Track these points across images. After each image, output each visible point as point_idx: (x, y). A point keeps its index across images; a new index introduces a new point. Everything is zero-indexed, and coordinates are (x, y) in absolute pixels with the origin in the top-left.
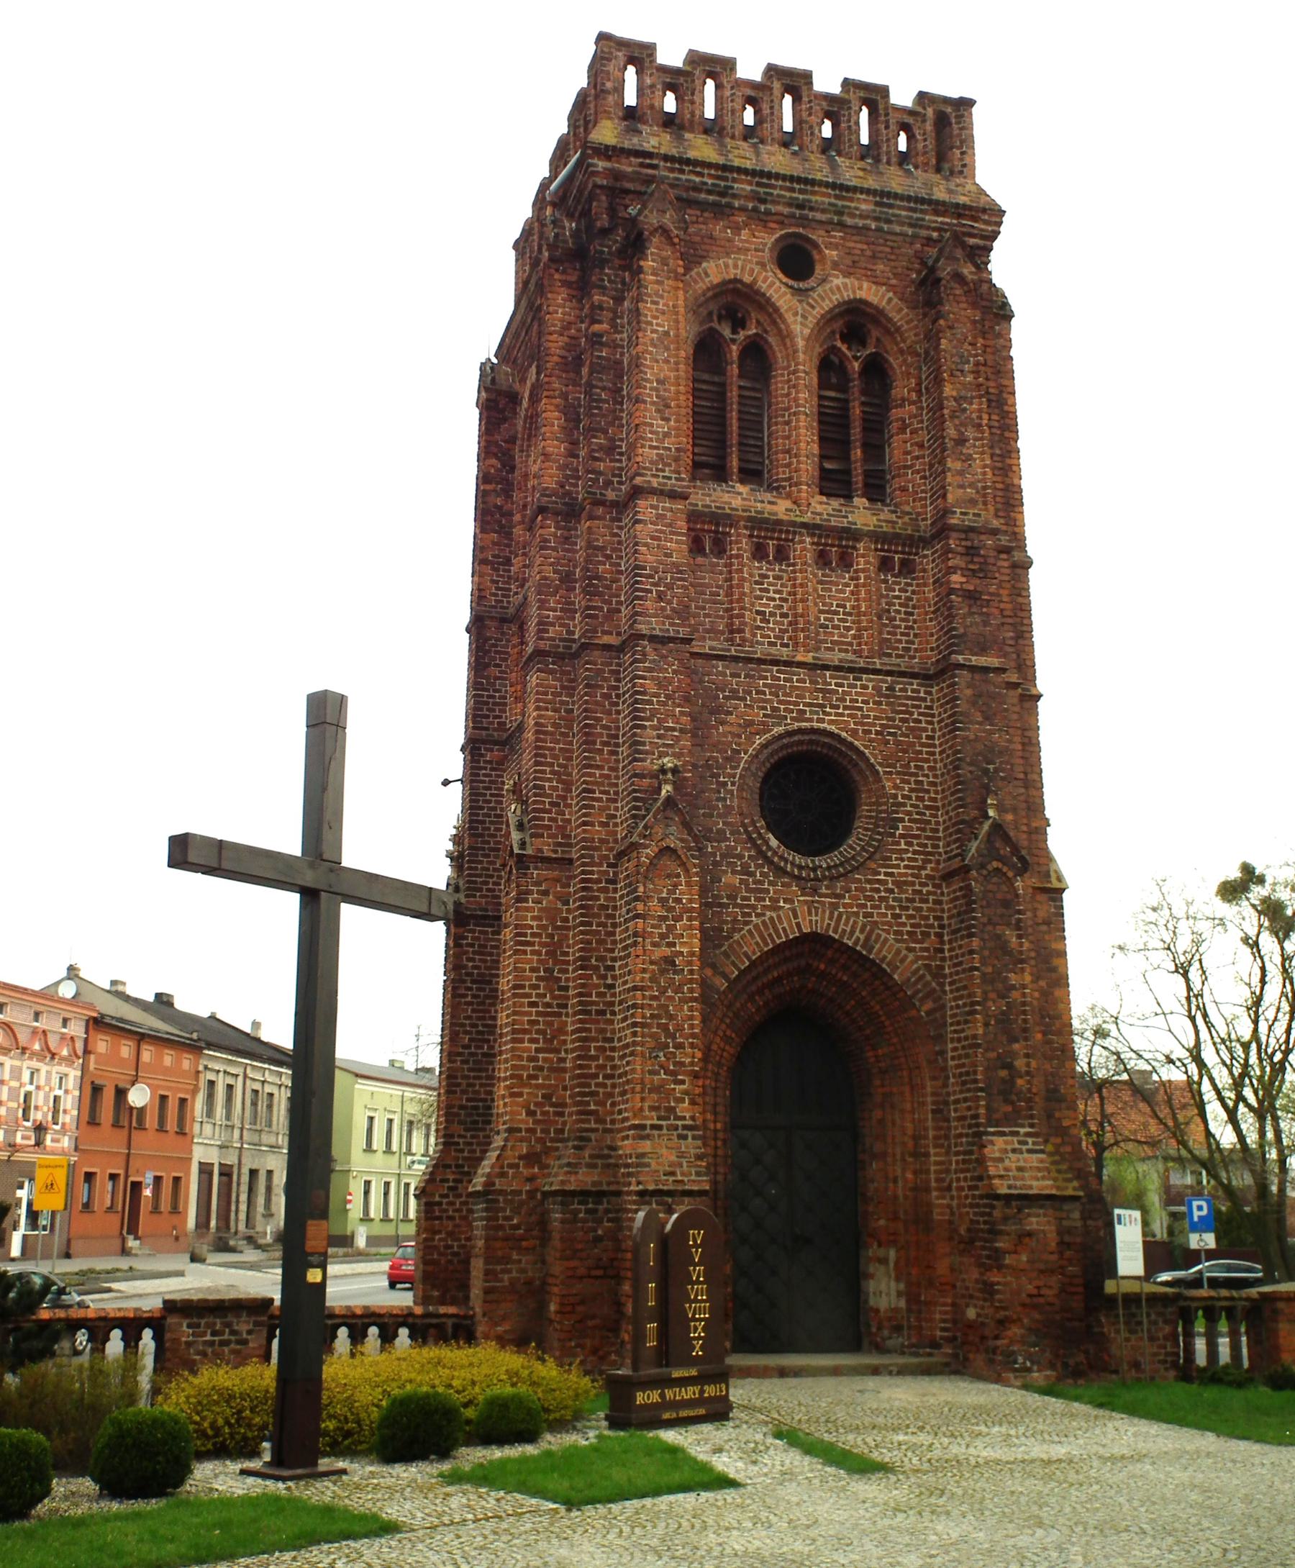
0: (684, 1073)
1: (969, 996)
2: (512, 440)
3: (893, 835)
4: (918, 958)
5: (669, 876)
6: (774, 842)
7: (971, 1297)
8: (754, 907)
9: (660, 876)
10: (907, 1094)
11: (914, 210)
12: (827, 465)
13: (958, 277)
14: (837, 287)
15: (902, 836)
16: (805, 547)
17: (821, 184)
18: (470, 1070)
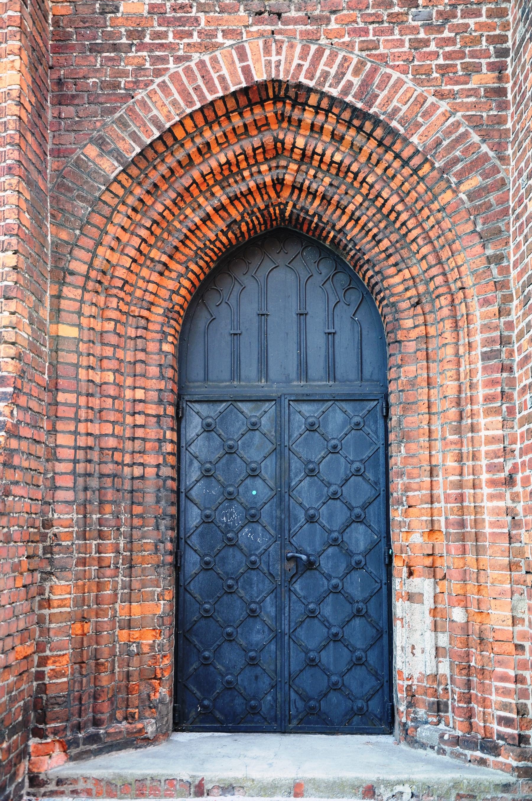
8: (171, 47)
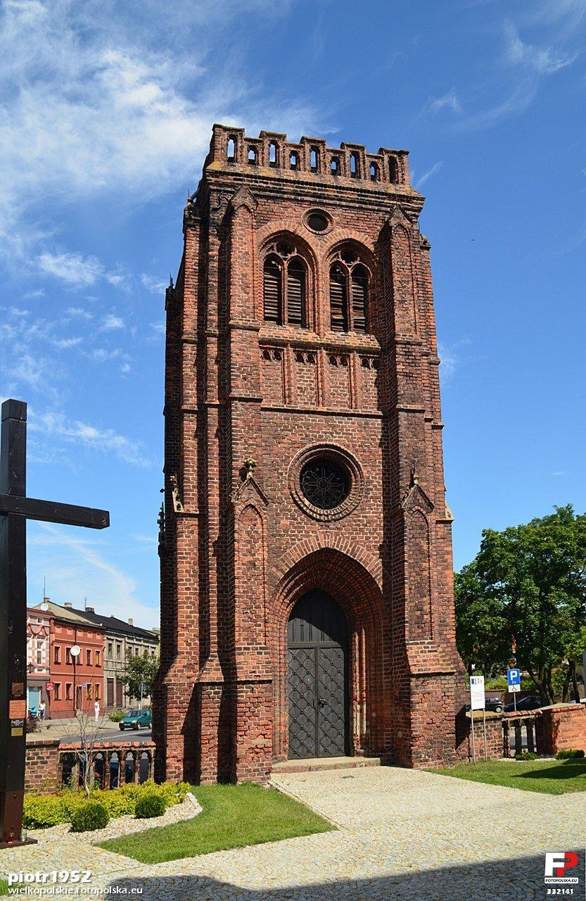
6: (307, 503)
7: (400, 726)
8: (297, 536)
10: (372, 628)
11: (379, 198)
12: (334, 317)
13: (402, 226)
14: (338, 233)
15: (372, 498)
17: (329, 186)
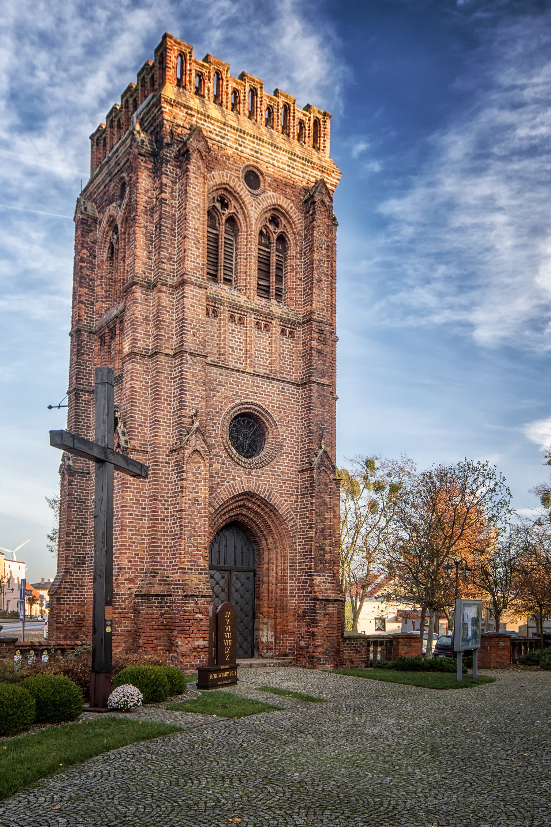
0: (201, 547)
1: (310, 521)
2: (94, 242)
3: (281, 452)
4: (288, 504)
5: (196, 463)
6: (234, 451)
7: (303, 637)
8: (226, 478)
9: (193, 462)
13: (323, 202)
15: (285, 453)
16: (250, 320)
18: (76, 541)
